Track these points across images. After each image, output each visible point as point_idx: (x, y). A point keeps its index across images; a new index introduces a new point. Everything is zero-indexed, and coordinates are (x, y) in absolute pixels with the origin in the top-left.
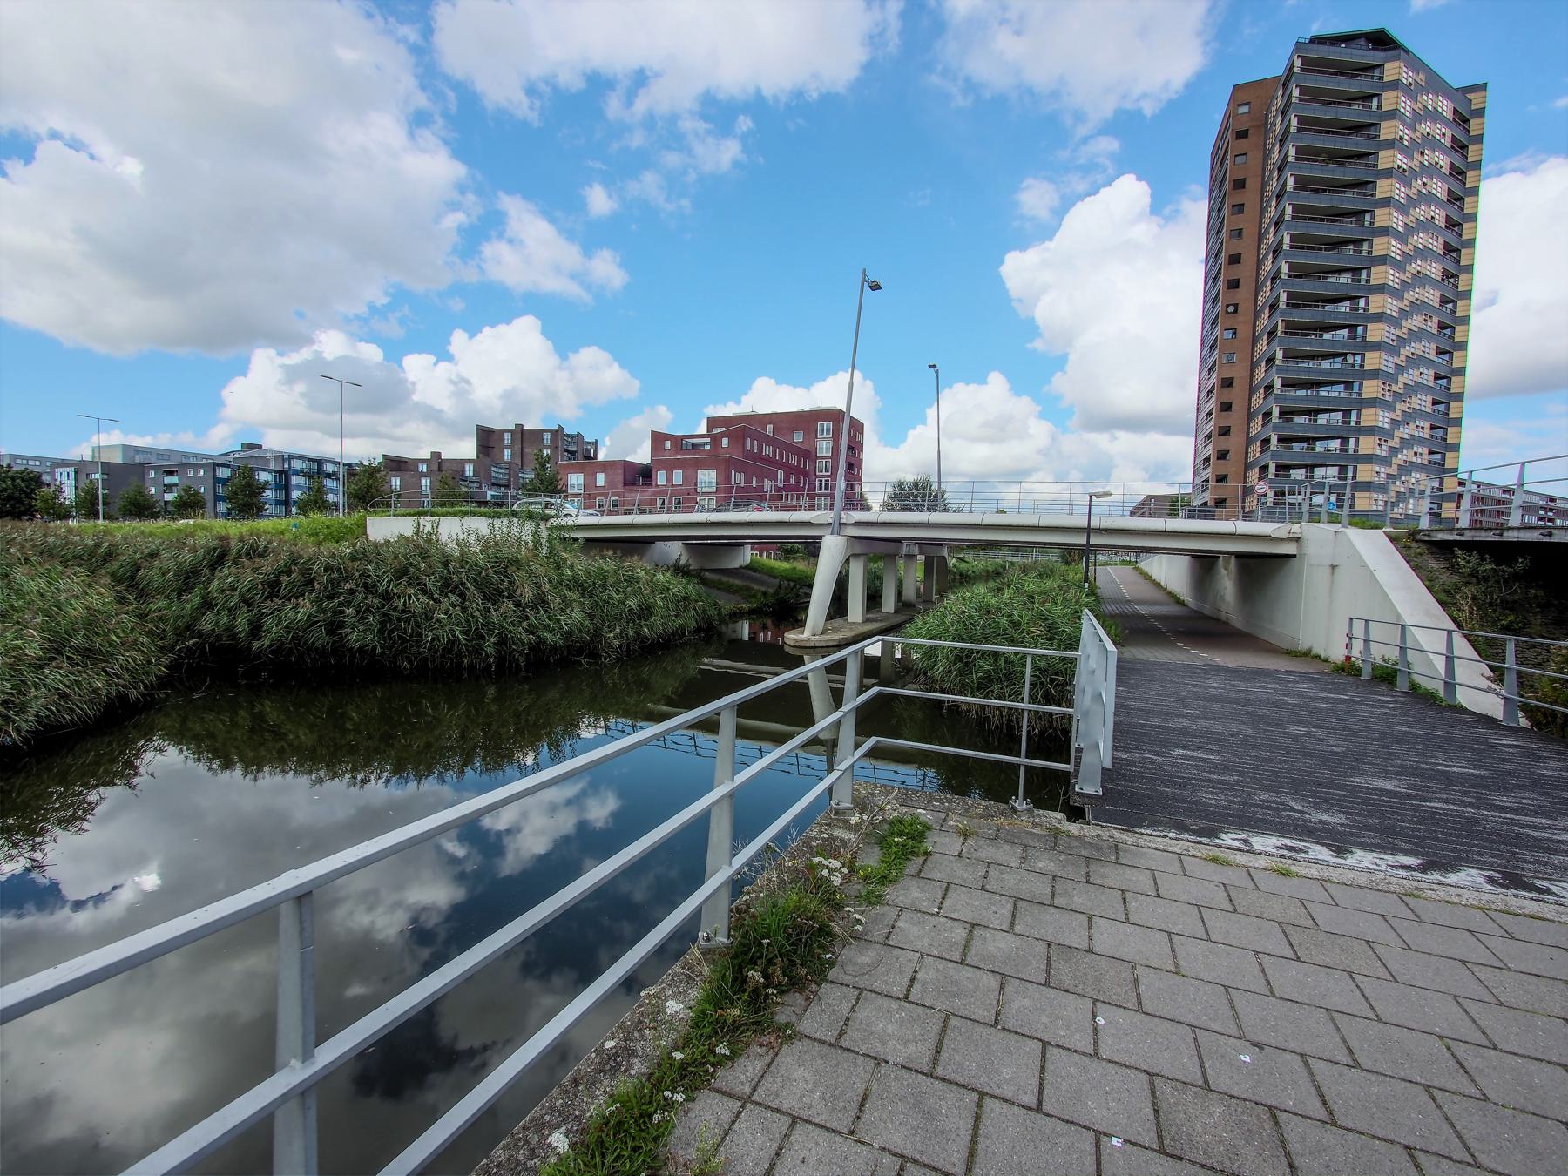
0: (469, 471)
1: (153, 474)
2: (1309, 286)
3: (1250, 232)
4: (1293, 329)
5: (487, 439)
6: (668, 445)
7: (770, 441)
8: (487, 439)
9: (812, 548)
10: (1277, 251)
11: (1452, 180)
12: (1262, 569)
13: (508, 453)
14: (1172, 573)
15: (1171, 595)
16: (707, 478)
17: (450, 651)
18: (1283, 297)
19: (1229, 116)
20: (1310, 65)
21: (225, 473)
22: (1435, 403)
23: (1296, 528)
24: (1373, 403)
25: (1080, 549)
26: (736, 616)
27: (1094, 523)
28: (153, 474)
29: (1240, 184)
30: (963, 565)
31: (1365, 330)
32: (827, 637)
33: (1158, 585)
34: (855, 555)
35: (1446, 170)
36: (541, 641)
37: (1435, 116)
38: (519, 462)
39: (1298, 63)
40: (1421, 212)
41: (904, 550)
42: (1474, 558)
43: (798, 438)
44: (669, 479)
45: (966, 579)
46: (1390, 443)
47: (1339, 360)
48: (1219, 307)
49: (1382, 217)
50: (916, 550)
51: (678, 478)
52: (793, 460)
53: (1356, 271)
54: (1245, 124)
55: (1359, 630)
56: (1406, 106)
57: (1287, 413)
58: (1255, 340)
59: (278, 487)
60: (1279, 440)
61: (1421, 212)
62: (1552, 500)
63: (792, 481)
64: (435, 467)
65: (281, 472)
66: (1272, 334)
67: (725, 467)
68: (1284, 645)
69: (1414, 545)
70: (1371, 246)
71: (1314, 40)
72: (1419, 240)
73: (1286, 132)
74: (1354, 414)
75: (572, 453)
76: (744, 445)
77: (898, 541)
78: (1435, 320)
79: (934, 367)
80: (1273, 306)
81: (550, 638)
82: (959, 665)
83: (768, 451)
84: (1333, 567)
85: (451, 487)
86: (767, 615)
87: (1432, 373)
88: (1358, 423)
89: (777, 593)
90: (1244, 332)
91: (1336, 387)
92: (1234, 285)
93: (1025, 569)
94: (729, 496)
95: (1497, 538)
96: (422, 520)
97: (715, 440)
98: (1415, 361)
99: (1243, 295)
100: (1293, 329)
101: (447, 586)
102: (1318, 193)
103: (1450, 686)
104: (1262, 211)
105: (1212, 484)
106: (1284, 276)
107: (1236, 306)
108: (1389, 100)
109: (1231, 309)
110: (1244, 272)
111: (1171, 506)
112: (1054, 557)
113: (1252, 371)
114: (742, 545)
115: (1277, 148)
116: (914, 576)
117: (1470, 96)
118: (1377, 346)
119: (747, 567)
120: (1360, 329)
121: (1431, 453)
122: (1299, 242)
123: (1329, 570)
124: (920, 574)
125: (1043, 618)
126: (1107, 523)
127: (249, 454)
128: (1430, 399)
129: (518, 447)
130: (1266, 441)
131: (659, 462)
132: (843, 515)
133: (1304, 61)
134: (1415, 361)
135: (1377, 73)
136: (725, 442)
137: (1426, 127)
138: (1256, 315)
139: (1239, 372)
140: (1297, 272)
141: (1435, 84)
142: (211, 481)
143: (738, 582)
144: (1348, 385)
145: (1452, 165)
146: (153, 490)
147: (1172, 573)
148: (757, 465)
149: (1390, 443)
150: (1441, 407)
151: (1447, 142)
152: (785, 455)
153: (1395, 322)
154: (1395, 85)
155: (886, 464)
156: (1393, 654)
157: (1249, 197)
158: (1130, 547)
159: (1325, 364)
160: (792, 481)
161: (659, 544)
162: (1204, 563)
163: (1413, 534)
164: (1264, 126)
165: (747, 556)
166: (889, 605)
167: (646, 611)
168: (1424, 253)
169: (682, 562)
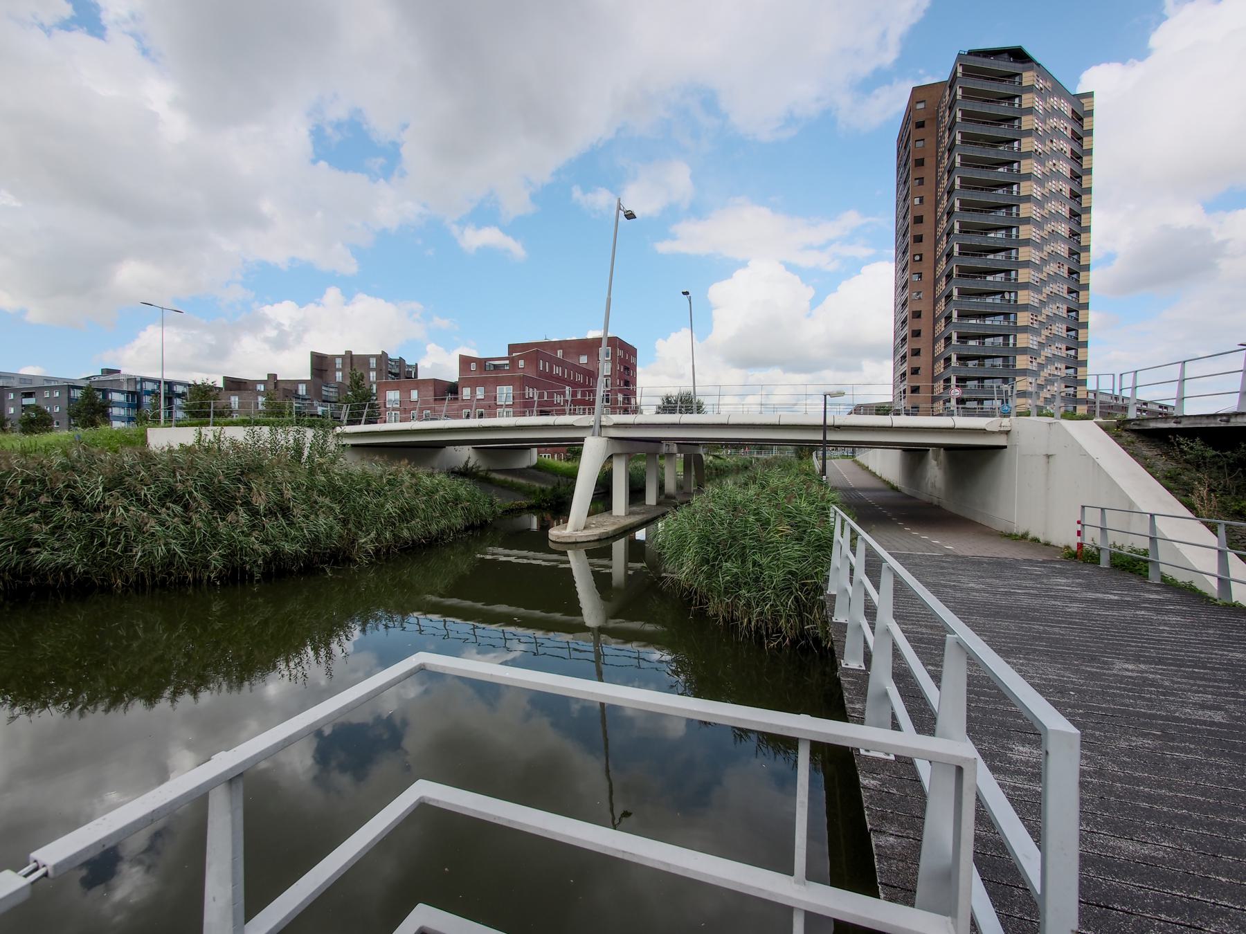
0: (302, 390)
1: (12, 396)
2: (976, 240)
3: (929, 198)
4: (966, 273)
5: (320, 364)
6: (473, 366)
7: (560, 363)
8: (320, 364)
9: (573, 449)
10: (950, 213)
11: (1073, 163)
12: (972, 461)
13: (339, 375)
14: (886, 465)
15: (888, 483)
16: (505, 393)
17: (171, 564)
18: (956, 248)
19: (910, 109)
20: (970, 71)
21: (77, 394)
22: (1068, 330)
23: (1005, 421)
24: (1025, 329)
25: (809, 445)
26: (516, 511)
27: (829, 421)
28: (12, 396)
29: (920, 163)
30: (718, 462)
31: (1017, 274)
32: (587, 532)
33: (874, 474)
34: (618, 455)
35: (1068, 155)
36: (277, 553)
37: (1058, 113)
38: (347, 386)
39: (960, 70)
40: (1053, 185)
41: (664, 449)
42: (1198, 445)
43: (584, 360)
44: (473, 393)
45: (721, 473)
46: (1039, 360)
47: (999, 297)
48: (908, 256)
49: (1026, 188)
50: (674, 449)
51: (480, 393)
52: (580, 378)
53: (1008, 228)
54: (922, 119)
55: (1093, 517)
56: (1039, 105)
57: (963, 338)
58: (936, 282)
59: (130, 406)
60: (959, 359)
61: (1053, 185)
62: (1145, 404)
63: (579, 397)
64: (272, 387)
65: (133, 393)
66: (949, 276)
67: (523, 382)
68: (1001, 527)
69: (1124, 434)
70: (1018, 210)
71: (970, 53)
72: (1053, 206)
73: (954, 122)
74: (1011, 338)
75: (396, 375)
76: (538, 366)
77: (658, 441)
78: (1066, 267)
79: (686, 293)
80: (949, 255)
81: (288, 547)
82: (705, 568)
83: (557, 370)
84: (1048, 456)
85: (279, 400)
86: (545, 509)
87: (1065, 307)
88: (1015, 345)
89: (554, 489)
90: (928, 276)
91: (997, 318)
92: (918, 239)
93: (768, 464)
94: (524, 406)
95: (1223, 424)
96: (204, 430)
97: (514, 361)
98: (1053, 297)
99: (926, 247)
100: (966, 273)
101: (170, 495)
102: (977, 165)
103: (1224, 583)
104: (938, 183)
105: (908, 394)
106: (956, 231)
107: (921, 255)
108: (1027, 100)
109: (917, 258)
110: (926, 229)
111: (882, 410)
112: (789, 452)
113: (935, 305)
114: (529, 448)
115: (947, 134)
116: (673, 472)
117: (1083, 101)
118: (1026, 286)
119: (534, 467)
120: (1013, 273)
121: (1067, 368)
122: (967, 206)
123: (1045, 459)
124: (680, 469)
125: (789, 515)
126: (840, 421)
127: (111, 377)
128: (1064, 327)
129: (348, 370)
130: (948, 360)
131: (466, 380)
132: (603, 418)
133: (965, 68)
134: (1053, 297)
135: (1017, 79)
136: (521, 363)
137: (1053, 122)
138: (936, 262)
139: (925, 307)
140: (966, 229)
141: (1058, 89)
142: (66, 401)
143: (522, 481)
144: (1007, 315)
145: (1072, 152)
146: (12, 411)
147: (886, 465)
148: (548, 382)
149: (1039, 360)
150: (1073, 333)
151: (1068, 133)
152: (566, 371)
153: (1038, 268)
154: (1030, 89)
155: (653, 383)
156: (1143, 544)
157: (928, 172)
158: (851, 441)
159: (989, 300)
160: (579, 397)
161: (450, 449)
162: (915, 455)
163: (1123, 423)
164: (936, 120)
165: (533, 457)
166: (651, 498)
167: (407, 513)
168: (1056, 216)
169: (470, 465)
